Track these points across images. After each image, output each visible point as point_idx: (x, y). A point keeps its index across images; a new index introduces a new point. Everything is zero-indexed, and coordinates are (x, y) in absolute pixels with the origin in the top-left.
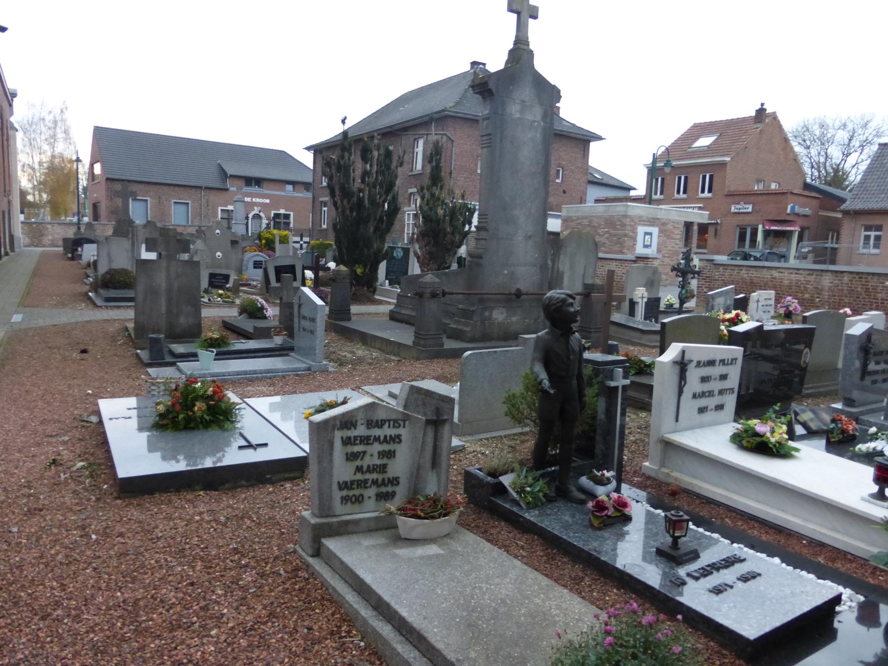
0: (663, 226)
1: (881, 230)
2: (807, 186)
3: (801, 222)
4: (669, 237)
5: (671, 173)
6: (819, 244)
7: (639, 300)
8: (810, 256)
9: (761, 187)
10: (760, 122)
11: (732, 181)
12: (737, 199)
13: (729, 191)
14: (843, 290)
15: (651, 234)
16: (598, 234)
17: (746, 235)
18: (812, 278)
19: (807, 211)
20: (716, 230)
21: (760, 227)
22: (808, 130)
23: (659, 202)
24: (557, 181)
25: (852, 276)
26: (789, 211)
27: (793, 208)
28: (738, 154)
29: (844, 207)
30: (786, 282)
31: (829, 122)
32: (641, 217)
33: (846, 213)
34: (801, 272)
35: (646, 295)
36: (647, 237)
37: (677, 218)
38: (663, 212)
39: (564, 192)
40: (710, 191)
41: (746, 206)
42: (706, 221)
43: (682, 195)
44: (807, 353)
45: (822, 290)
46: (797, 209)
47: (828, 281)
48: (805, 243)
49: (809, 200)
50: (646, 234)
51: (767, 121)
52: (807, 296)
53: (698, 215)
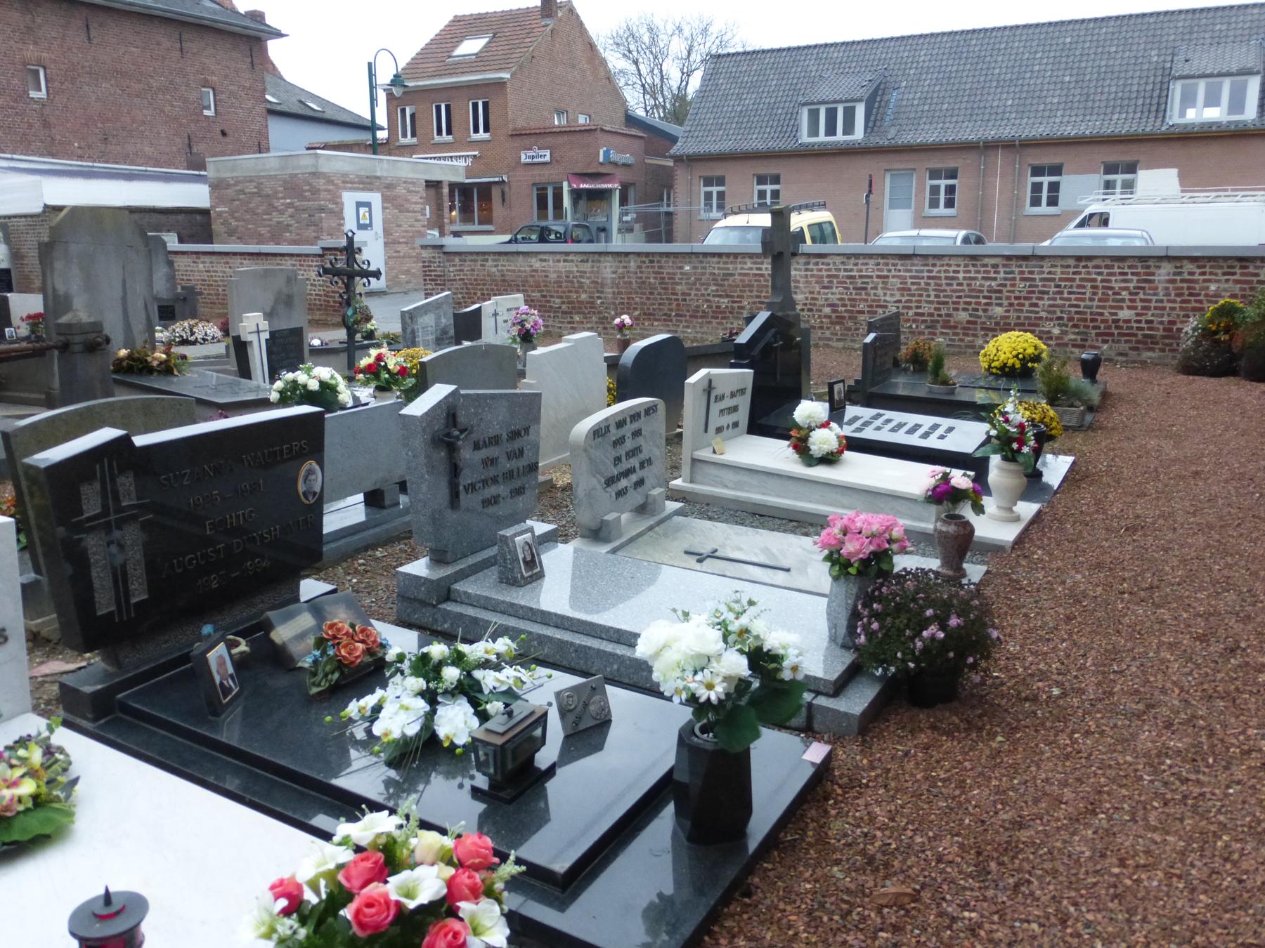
0: (388, 189)
1: (954, 177)
2: (631, 120)
3: (621, 174)
4: (401, 209)
5: (429, 98)
6: (650, 208)
7: (252, 338)
8: (637, 227)
9: (564, 122)
10: (549, 16)
11: (518, 110)
12: (527, 141)
13: (515, 130)
14: (631, 283)
15: (368, 205)
16: (276, 209)
17: (545, 199)
18: (587, 267)
19: (627, 158)
20: (503, 193)
21: (565, 184)
22: (632, 35)
23: (409, 150)
24: (206, 113)
25: (639, 259)
26: (601, 160)
27: (607, 154)
28: (521, 67)
29: (676, 149)
30: (553, 276)
31: (658, 22)
32: (345, 175)
33: (678, 159)
34: (570, 258)
35: (264, 325)
36: (362, 210)
37: (411, 175)
38: (385, 165)
39: (224, 133)
40: (486, 130)
41: (542, 153)
42: (461, 179)
43: (445, 138)
44: (310, 472)
45: (603, 285)
46: (614, 156)
47: (608, 270)
48: (631, 207)
49: (630, 140)
50: (359, 205)
51: (560, 14)
52: (584, 296)
53: (453, 167)
